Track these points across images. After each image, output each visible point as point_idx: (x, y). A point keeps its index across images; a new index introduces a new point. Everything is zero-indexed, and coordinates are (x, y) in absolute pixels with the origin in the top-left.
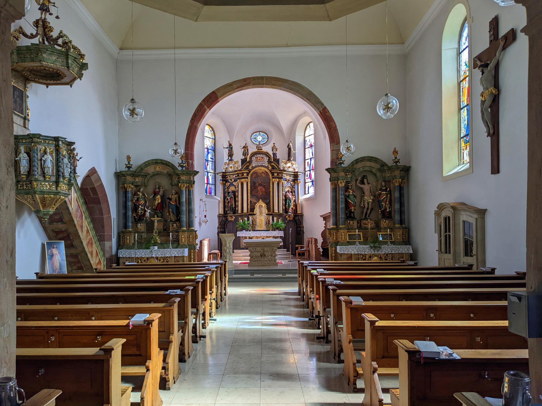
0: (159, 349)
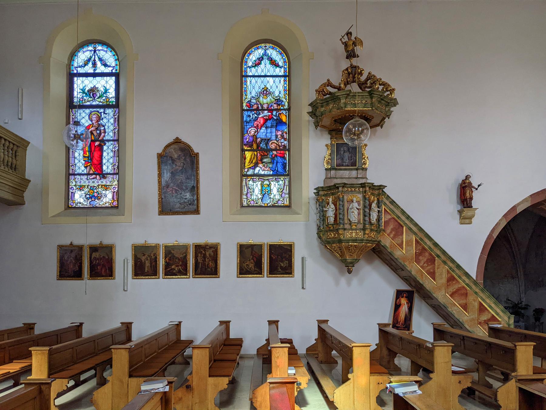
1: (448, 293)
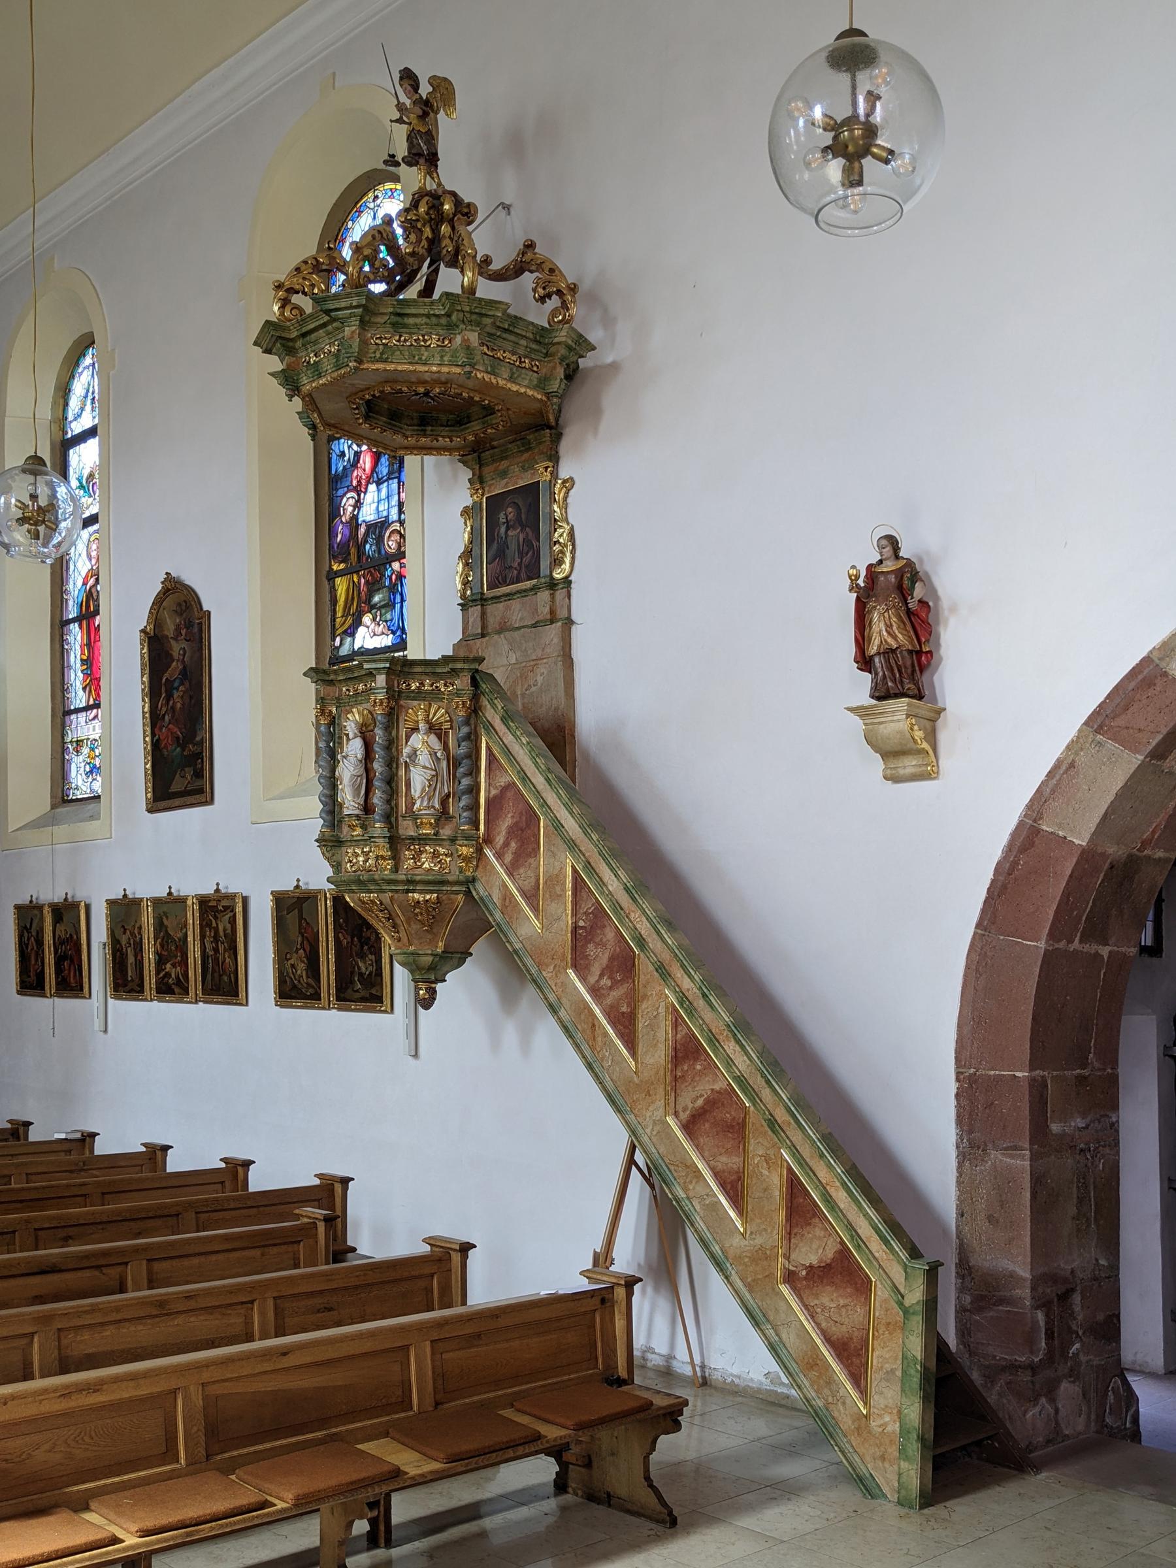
1: (676, 1114)
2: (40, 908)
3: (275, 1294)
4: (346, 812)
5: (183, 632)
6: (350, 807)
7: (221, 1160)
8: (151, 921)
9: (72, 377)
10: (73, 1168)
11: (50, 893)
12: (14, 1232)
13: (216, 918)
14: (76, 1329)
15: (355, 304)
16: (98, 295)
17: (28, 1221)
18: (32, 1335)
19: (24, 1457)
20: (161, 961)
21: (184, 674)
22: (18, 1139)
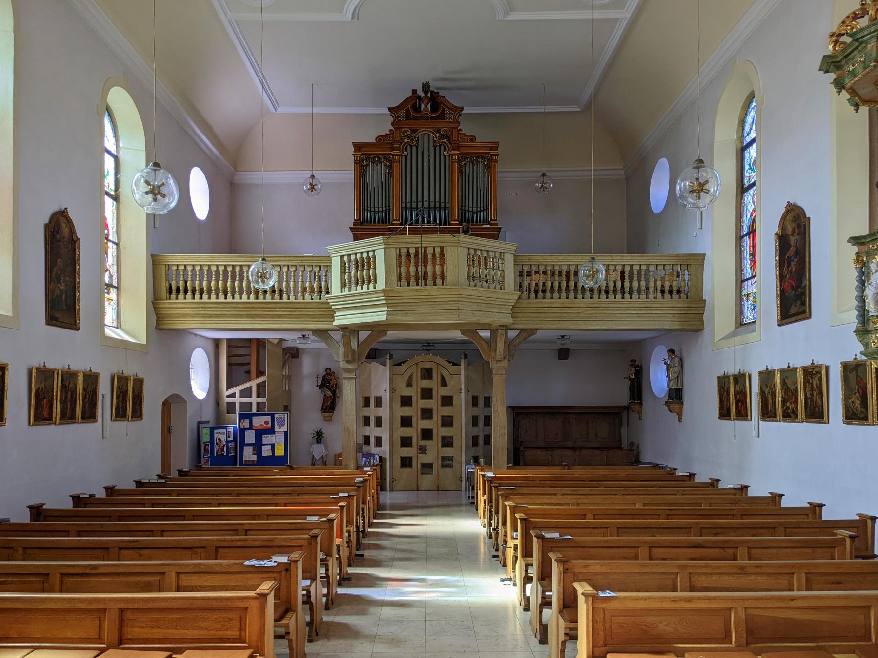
0: (758, 490)
2: (728, 377)
3: (807, 571)
4: (870, 314)
5: (796, 231)
6: (873, 311)
7: (807, 503)
8: (780, 381)
9: (746, 114)
10: (733, 502)
11: (733, 370)
12: (691, 528)
13: (812, 378)
14: (699, 574)
15: (872, 30)
16: (755, 68)
17: (697, 524)
18: (677, 573)
19: (654, 626)
20: (784, 401)
21: (797, 253)
22: (714, 487)
